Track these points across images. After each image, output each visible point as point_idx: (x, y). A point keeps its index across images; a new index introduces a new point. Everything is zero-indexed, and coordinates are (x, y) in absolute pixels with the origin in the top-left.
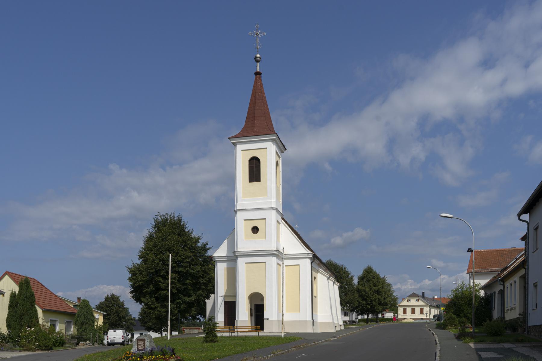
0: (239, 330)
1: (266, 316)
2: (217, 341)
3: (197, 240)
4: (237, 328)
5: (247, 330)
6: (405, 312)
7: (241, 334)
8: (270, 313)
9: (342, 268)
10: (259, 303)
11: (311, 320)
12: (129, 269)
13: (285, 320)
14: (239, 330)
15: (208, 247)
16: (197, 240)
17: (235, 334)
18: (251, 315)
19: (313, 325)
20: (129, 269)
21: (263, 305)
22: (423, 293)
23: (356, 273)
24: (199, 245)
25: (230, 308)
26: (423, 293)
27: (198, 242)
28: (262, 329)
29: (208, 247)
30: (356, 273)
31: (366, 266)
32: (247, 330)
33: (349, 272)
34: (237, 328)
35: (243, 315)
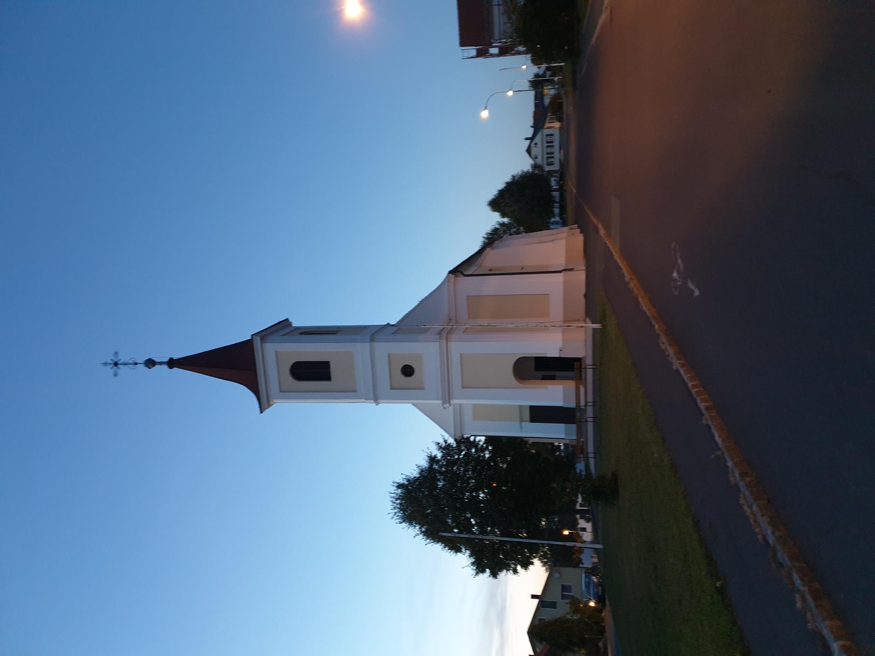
0: (582, 404)
1: (555, 354)
2: (615, 477)
3: (432, 459)
4: (578, 405)
5: (582, 389)
6: (551, 164)
7: (590, 399)
8: (551, 345)
9: (487, 238)
10: (532, 365)
11: (562, 274)
12: (477, 573)
13: (518, 423)
14: (582, 404)
15: (441, 441)
16: (432, 459)
17: (590, 412)
18: (553, 378)
19: (572, 270)
20: (477, 573)
21: (536, 358)
22: (527, 139)
23: (495, 219)
24: (439, 455)
25: (539, 414)
26: (527, 139)
27: (435, 457)
28: (579, 360)
29: (441, 441)
30: (495, 219)
31: (488, 209)
32: (582, 389)
33: (493, 228)
34: (578, 405)
35: (554, 394)
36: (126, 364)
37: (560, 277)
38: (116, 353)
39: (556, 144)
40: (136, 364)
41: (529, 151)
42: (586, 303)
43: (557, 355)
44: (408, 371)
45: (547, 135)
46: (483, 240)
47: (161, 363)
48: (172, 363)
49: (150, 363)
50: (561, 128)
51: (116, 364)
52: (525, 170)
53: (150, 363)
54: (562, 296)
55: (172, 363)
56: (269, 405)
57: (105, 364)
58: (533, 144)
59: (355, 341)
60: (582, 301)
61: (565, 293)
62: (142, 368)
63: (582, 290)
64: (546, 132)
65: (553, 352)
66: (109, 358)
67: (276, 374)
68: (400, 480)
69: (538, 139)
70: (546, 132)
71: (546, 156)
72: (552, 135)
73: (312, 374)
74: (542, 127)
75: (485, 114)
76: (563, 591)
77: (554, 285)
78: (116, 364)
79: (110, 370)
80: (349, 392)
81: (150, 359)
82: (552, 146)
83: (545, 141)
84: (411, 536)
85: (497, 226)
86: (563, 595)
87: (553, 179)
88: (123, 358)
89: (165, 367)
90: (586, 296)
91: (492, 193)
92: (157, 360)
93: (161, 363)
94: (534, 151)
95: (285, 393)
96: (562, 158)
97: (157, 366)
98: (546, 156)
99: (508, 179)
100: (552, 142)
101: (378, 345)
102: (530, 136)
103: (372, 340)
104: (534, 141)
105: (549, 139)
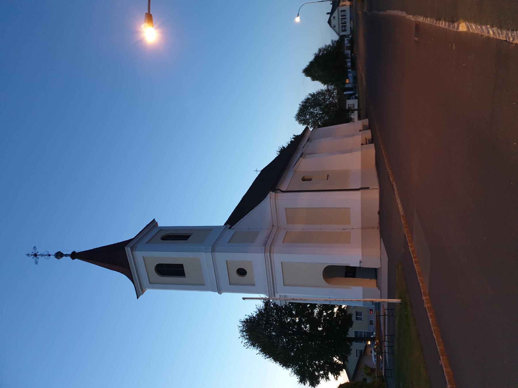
1: (356, 264)
8: (352, 257)
11: (359, 192)
19: (368, 188)
22: (328, 14)
26: (328, 14)
28: (376, 270)
36: (42, 255)
37: (358, 195)
38: (35, 247)
39: (348, 17)
40: (49, 255)
41: (329, 22)
42: (380, 219)
43: (357, 265)
44: (242, 272)
45: (342, 11)
46: (299, 106)
47: (66, 255)
48: (74, 255)
49: (59, 255)
50: (351, 6)
51: (36, 255)
52: (328, 44)
53: (59, 255)
54: (360, 217)
55: (74, 255)
56: (143, 292)
57: (28, 255)
58: (332, 18)
59: (200, 251)
60: (378, 216)
61: (362, 207)
62: (53, 258)
63: (377, 208)
64: (341, 8)
65: (355, 263)
66: (31, 251)
67: (155, 233)
68: (243, 318)
69: (335, 14)
70: (341, 8)
71: (341, 25)
72: (345, 11)
73: (171, 273)
74: (338, 5)
75: (298, 19)
76: (356, 315)
77: (352, 201)
78: (36, 255)
79: (31, 259)
80: (199, 285)
81: (59, 252)
82: (345, 18)
83: (340, 22)
84: (254, 355)
85: (310, 97)
86: (356, 318)
87: (346, 39)
88: (40, 251)
89: (69, 258)
90: (379, 213)
91: (305, 64)
92: (64, 253)
93: (66, 255)
94: (333, 22)
95: (154, 284)
96: (352, 27)
97: (64, 257)
98: (341, 18)
99: (316, 51)
100: (345, 16)
101: (218, 255)
102: (330, 11)
103: (213, 251)
104: (333, 16)
105: (343, 13)
